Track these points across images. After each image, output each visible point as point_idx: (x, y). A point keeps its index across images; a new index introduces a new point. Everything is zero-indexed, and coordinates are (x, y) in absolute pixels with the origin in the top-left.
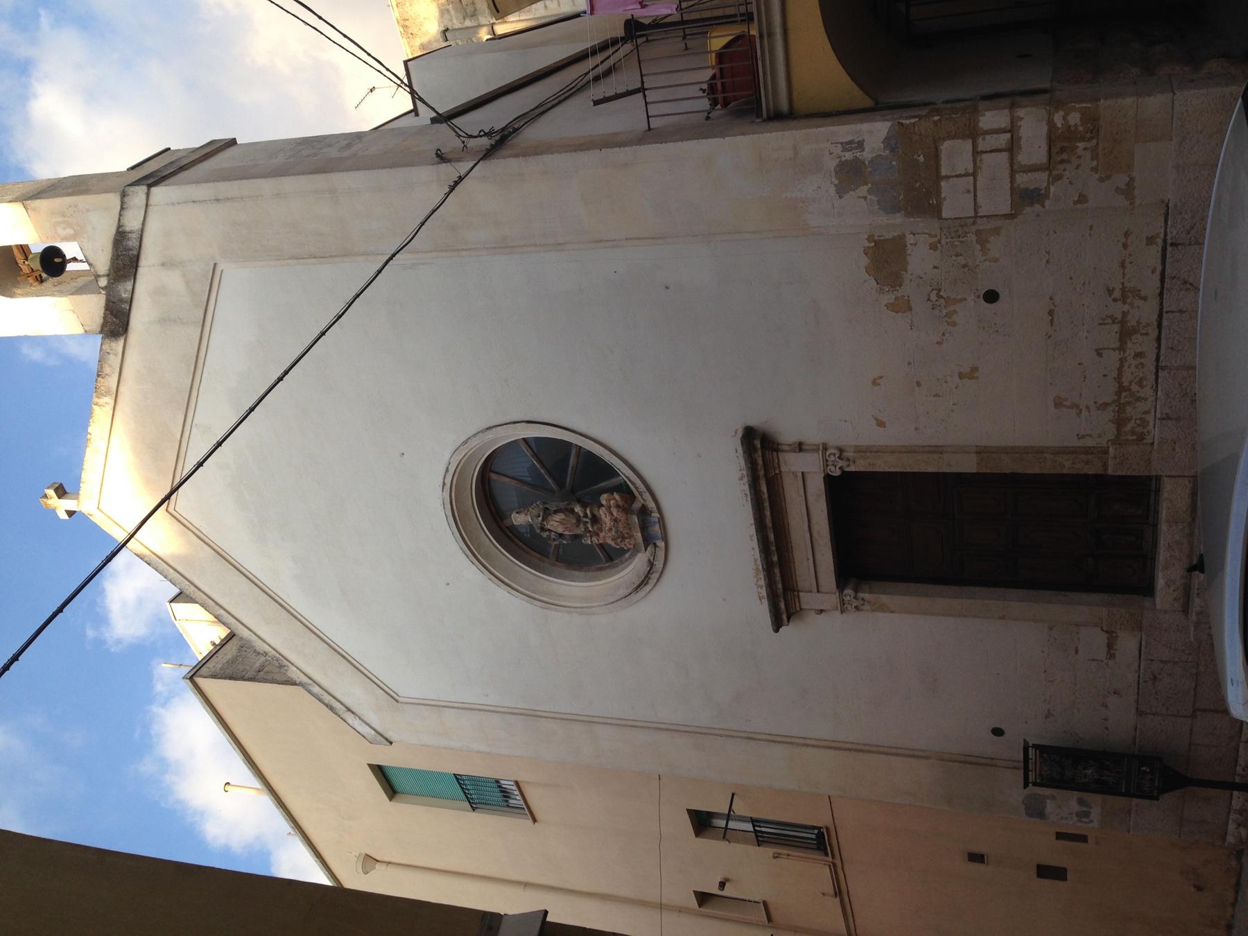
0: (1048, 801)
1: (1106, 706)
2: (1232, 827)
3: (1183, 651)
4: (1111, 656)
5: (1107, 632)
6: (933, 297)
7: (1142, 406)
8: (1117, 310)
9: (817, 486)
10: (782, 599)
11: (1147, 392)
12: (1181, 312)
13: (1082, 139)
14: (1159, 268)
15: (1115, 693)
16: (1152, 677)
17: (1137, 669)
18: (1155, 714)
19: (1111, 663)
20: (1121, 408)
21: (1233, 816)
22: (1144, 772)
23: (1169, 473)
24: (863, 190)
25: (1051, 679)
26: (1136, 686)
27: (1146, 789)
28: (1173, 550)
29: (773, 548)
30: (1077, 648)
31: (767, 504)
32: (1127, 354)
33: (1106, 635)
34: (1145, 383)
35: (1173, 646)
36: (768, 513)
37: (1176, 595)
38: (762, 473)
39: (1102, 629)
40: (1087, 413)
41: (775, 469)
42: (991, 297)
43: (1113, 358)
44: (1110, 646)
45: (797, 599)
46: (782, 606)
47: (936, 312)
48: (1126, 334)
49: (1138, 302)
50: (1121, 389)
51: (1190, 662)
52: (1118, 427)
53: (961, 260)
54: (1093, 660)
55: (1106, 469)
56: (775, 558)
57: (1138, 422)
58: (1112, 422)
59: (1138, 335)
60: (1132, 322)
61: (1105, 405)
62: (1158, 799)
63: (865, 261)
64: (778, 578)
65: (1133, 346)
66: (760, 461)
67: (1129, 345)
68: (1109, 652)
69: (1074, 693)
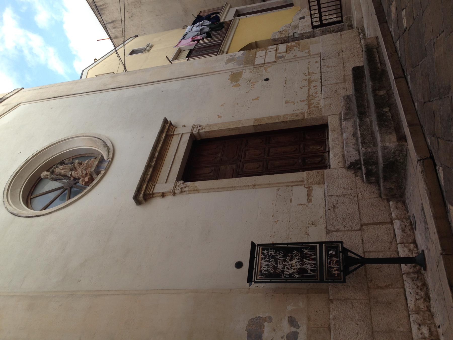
0: (266, 324)
1: (308, 234)
2: (414, 328)
3: (348, 189)
4: (309, 201)
5: (307, 188)
6: (248, 82)
7: (317, 99)
8: (307, 78)
9: (186, 138)
10: (146, 183)
11: (319, 95)
12: (327, 72)
13: (296, 46)
14: (320, 67)
15: (313, 224)
16: (333, 206)
17: (324, 206)
18: (337, 231)
19: (310, 205)
20: (310, 101)
21: (413, 317)
22: (332, 256)
23: (329, 114)
24: (233, 62)
25: (276, 220)
26: (325, 217)
27: (334, 272)
28: (335, 141)
29: (155, 159)
30: (291, 199)
31: (161, 142)
32: (311, 87)
33: (306, 189)
34: (317, 93)
35: (341, 186)
36: (160, 145)
37: (339, 160)
38: (165, 131)
39: (304, 186)
40: (297, 104)
41: (171, 132)
42: (267, 80)
43: (306, 89)
44: (309, 195)
45: (153, 187)
46: (145, 186)
47: (248, 85)
48: (310, 82)
49: (313, 75)
50: (309, 96)
51: (353, 194)
52: (309, 106)
53: (259, 74)
54: (300, 204)
55: (304, 117)
56: (153, 164)
57: (316, 104)
58: (307, 105)
59: (314, 82)
60: (312, 79)
61: (304, 101)
62: (344, 282)
63: (229, 77)
64: (150, 173)
65: (312, 85)
66: (167, 127)
67: (311, 84)
68: (308, 198)
69: (289, 228)
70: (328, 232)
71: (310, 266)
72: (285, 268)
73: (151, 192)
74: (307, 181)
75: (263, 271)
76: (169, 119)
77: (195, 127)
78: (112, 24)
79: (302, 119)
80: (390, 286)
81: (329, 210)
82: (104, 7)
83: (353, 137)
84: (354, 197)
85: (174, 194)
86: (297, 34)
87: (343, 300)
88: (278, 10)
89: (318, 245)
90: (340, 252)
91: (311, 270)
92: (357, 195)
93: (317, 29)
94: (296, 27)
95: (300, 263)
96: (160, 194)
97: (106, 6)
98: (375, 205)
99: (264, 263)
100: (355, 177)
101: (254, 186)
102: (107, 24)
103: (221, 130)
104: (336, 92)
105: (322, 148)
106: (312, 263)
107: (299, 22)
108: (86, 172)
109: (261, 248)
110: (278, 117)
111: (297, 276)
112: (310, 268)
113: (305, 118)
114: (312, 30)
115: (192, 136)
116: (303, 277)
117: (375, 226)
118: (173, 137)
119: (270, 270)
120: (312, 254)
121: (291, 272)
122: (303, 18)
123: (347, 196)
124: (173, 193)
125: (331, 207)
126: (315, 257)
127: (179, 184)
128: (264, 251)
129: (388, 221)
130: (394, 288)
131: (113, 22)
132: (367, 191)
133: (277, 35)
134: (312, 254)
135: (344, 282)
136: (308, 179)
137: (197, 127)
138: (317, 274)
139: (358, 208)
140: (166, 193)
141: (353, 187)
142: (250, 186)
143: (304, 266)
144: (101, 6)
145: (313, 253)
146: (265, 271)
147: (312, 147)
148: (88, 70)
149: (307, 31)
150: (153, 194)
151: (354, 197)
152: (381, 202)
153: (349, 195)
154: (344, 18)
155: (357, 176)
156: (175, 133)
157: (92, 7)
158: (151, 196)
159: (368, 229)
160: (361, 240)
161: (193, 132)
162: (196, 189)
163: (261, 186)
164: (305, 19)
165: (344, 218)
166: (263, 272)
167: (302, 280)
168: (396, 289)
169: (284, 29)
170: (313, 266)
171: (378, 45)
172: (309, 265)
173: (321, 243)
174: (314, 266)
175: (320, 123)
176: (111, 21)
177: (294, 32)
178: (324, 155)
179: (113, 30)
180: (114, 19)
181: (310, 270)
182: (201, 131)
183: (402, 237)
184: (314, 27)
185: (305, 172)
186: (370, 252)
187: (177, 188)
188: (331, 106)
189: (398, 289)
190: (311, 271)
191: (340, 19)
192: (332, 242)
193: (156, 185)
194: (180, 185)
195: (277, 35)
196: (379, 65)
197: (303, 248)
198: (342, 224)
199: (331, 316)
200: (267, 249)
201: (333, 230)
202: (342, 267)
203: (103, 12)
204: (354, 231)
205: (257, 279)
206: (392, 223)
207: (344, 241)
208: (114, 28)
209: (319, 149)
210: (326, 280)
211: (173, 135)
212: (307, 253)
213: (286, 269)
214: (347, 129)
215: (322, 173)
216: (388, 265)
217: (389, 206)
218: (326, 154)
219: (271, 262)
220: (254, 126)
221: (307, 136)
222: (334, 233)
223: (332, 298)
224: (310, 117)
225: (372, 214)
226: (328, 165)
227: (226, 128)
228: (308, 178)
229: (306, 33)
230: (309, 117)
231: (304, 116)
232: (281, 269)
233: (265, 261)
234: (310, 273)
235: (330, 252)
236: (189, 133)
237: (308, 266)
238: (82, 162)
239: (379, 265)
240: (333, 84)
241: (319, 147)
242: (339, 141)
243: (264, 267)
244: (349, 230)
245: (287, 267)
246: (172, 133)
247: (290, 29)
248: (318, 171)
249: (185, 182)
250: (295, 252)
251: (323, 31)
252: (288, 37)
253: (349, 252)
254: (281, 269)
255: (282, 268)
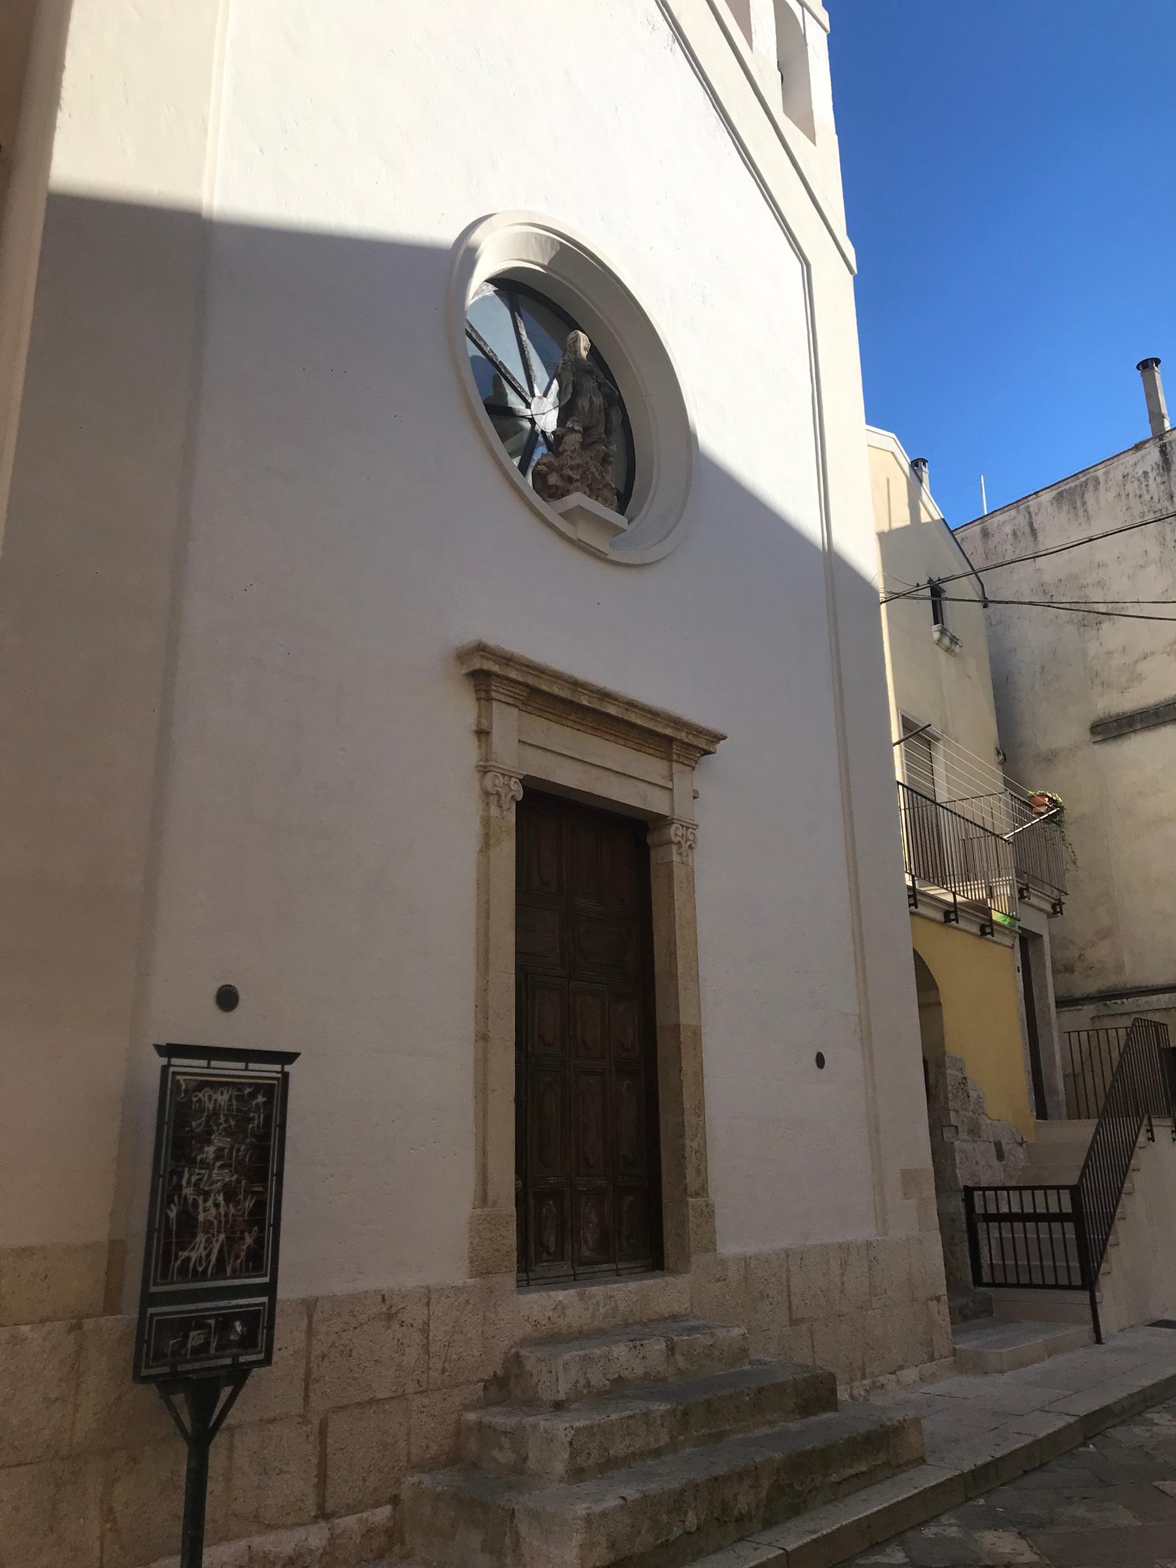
9: (656, 803)
28: (605, 1305)
41: (678, 755)
45: (510, 701)
70: (309, 1306)
71: (201, 1257)
72: (203, 1171)
73: (494, 694)
74: (485, 1220)
75: (200, 1095)
76: (721, 746)
77: (690, 830)
78: (1027, 529)
79: (685, 1189)
80: (108, 1526)
81: (384, 1300)
82: (1081, 512)
83: (615, 1380)
84: (419, 1381)
85: (484, 771)
86: (953, 1137)
87: (76, 1367)
88: (1029, 1067)
89: (266, 1280)
90: (235, 1357)
91: (188, 1259)
92: (421, 1392)
93: (961, 1204)
94: (975, 1131)
95: (212, 1223)
96: (485, 723)
97: (1082, 520)
98: (384, 1456)
99: (226, 1097)
100: (481, 1380)
101: (483, 1037)
102: (1027, 515)
103: (671, 908)
104: (763, 1296)
105: (586, 1252)
106: (210, 1261)
107: (990, 1142)
108: (578, 480)
109: (275, 1082)
110: (700, 1108)
111: (173, 1214)
112: (194, 1256)
113: (690, 1199)
114: (962, 1187)
115: (661, 821)
116: (168, 1231)
117: (315, 1461)
118: (662, 758)
119: (201, 1117)
120: (239, 1261)
121: (188, 1191)
122: (1000, 1155)
123: (422, 1356)
124: (485, 767)
125: (391, 1307)
126: (229, 1270)
127: (514, 787)
128: (264, 1096)
129: (327, 1505)
130: (102, 1539)
131: (1033, 532)
132: (433, 1425)
133: (954, 1072)
134: (239, 1261)
135: (139, 1379)
136: (489, 1222)
137: (688, 840)
138: (173, 1283)
139: (380, 1396)
140: (487, 740)
141: (450, 1376)
142: (486, 1024)
143: (201, 1238)
144: (1084, 504)
145: (241, 1264)
146: (200, 1101)
147: (594, 1217)
148: (893, 453)
149: (957, 1171)
150: (490, 699)
151: (419, 1381)
152: (391, 1476)
153: (426, 1365)
154: (990, 1291)
155: (485, 1388)
156: (675, 765)
157: (1080, 475)
158: (483, 695)
159: (308, 1436)
160: (271, 1415)
161: (675, 826)
162: (492, 841)
163: (483, 1063)
164: (996, 1163)
165: (351, 1350)
166: (196, 1096)
167: (159, 1231)
168: (97, 1544)
169: (973, 1094)
170: (200, 1265)
171: (899, 1466)
172: (204, 1254)
173: (270, 1289)
174: (200, 1269)
175: (669, 1246)
176: (1036, 526)
177: (960, 1130)
178: (563, 1259)
179: (1008, 529)
180: (1040, 535)
181: (189, 1256)
182: (674, 848)
183: (271, 1557)
184: (968, 1191)
185: (512, 1210)
186: (231, 1448)
187: (500, 780)
188: (719, 1284)
189: (97, 1553)
190: (183, 1261)
191: (986, 1278)
192: (271, 1326)
193: (516, 711)
194: (511, 790)
195: (954, 1072)
196: (834, 1477)
197: (262, 1230)
198: (333, 1345)
199: (25, 1329)
200: (268, 1104)
201: (315, 1316)
202: (188, 1367)
203: (1065, 508)
204: (307, 1386)
205: (174, 1073)
206: (323, 1515)
207: (272, 1368)
208: (1014, 533)
209: (586, 1243)
210: (148, 1315)
211: (671, 760)
212: (244, 1244)
213: (198, 1174)
214: (640, 1356)
215: (506, 1267)
216: (182, 1514)
217: (377, 1504)
218: (565, 1268)
219: (227, 1121)
220: (678, 1026)
221: (630, 1198)
222: (306, 1321)
223: (85, 1328)
224: (691, 1212)
225: (358, 1446)
226: (531, 1275)
227: (678, 933)
228: (493, 1222)
229: (954, 1166)
230: (690, 1210)
231: (696, 1194)
232: (199, 1157)
233: (230, 1099)
234: (176, 1259)
235: (238, 1326)
236: (673, 814)
237: (201, 1249)
238: (610, 463)
239: (182, 1482)
240: (788, 1285)
241: (590, 1244)
242: (605, 1317)
243: (210, 1097)
244: (308, 1371)
245: (205, 1178)
246: (675, 757)
247: (971, 1114)
248: (515, 1255)
249: (517, 803)
250: (251, 1199)
251: (953, 1220)
252: (948, 1110)
253: (234, 1390)
254: (199, 1157)
255: (202, 1159)
